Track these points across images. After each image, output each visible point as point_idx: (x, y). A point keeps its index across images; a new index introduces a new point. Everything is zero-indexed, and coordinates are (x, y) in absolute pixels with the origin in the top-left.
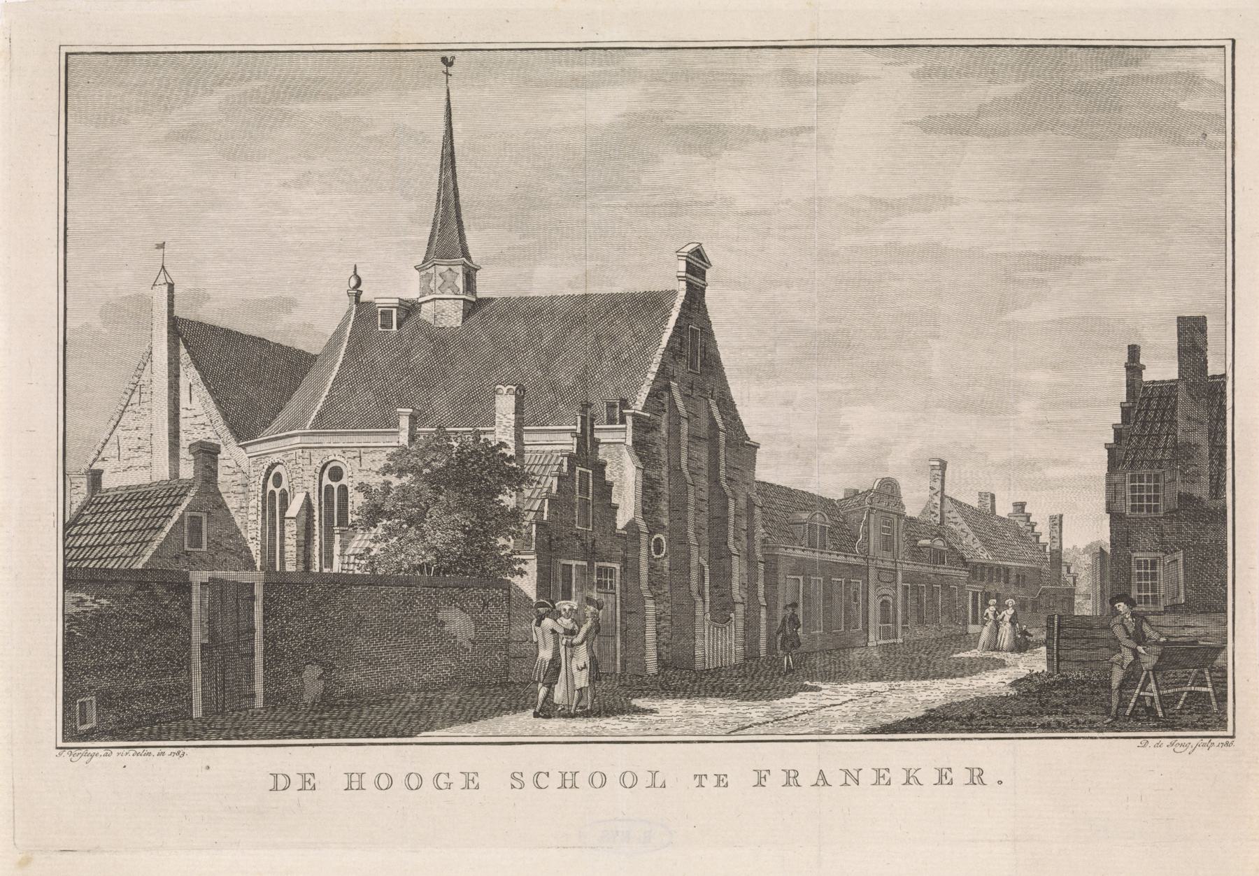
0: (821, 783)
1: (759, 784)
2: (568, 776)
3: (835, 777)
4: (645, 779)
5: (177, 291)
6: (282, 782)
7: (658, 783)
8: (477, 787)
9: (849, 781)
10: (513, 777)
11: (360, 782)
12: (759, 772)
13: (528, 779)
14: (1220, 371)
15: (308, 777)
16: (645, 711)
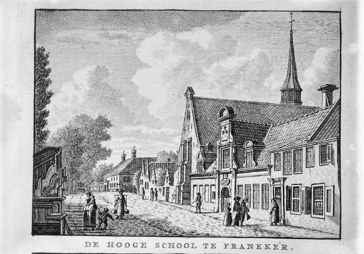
0: (242, 248)
1: (225, 248)
2: (111, 244)
3: (246, 246)
4: (191, 246)
5: (293, 184)
6: (88, 244)
7: (194, 247)
8: (261, 248)
9: (250, 247)
10: (156, 244)
11: (87, 244)
12: (258, 245)
13: (161, 245)
14: (338, 87)
15: (214, 245)
16: (160, 229)
